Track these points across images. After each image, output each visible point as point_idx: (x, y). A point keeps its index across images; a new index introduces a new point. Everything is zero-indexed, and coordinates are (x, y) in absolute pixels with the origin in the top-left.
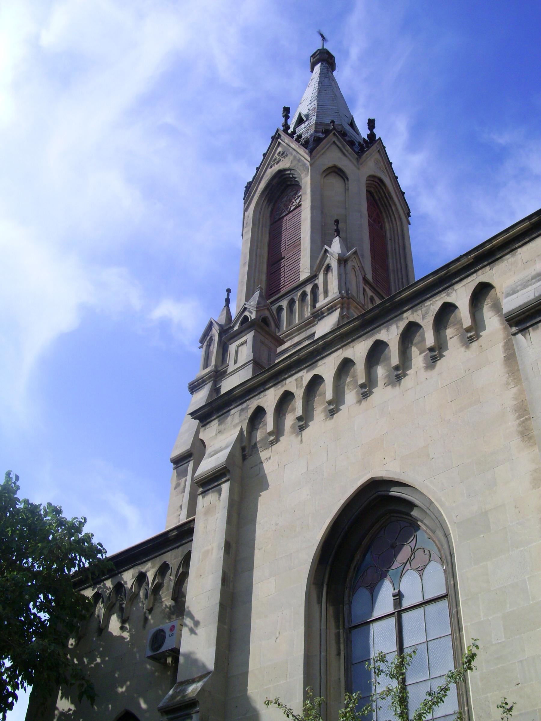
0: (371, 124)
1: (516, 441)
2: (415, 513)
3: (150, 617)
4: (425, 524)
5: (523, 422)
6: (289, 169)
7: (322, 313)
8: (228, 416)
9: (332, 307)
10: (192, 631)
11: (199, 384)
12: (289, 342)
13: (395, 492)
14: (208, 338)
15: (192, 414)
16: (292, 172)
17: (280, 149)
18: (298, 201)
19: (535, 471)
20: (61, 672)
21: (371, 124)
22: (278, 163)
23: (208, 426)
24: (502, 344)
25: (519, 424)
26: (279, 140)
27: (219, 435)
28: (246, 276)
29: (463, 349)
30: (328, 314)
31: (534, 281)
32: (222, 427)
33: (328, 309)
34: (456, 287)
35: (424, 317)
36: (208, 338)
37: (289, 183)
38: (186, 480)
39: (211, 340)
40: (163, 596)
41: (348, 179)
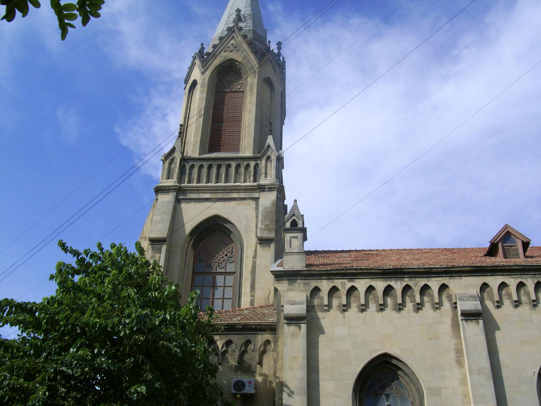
0: (279, 44)
1: (454, 363)
2: (399, 372)
3: (220, 367)
4: (404, 380)
5: (458, 356)
6: (240, 63)
7: (264, 188)
8: (295, 283)
9: (271, 188)
10: (289, 395)
11: (164, 190)
12: (237, 194)
13: (394, 362)
14: (171, 158)
15: (271, 271)
16: (241, 65)
17: (233, 42)
18: (239, 86)
19: (462, 379)
20: (238, 402)
21: (279, 44)
22: (231, 51)
23: (280, 282)
24: (450, 317)
25: (456, 357)
26: (233, 34)
27: (289, 291)
28: (201, 126)
29: (432, 311)
30: (268, 191)
31: (471, 299)
32: (291, 287)
33: (269, 188)
34: (432, 279)
35: (415, 285)
36: (171, 158)
37: (234, 69)
38: (160, 257)
39: (173, 160)
40: (229, 358)
41: (274, 91)
